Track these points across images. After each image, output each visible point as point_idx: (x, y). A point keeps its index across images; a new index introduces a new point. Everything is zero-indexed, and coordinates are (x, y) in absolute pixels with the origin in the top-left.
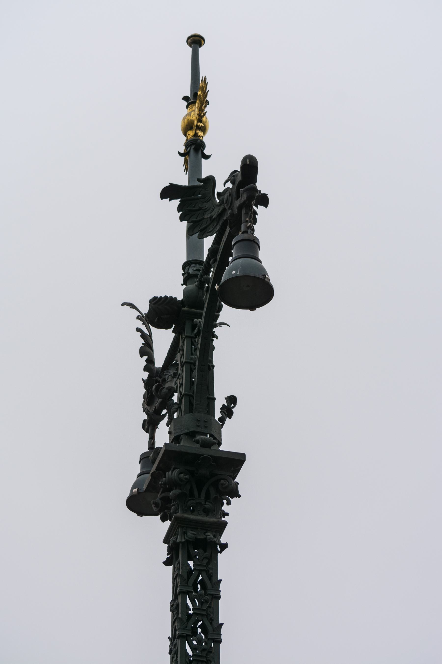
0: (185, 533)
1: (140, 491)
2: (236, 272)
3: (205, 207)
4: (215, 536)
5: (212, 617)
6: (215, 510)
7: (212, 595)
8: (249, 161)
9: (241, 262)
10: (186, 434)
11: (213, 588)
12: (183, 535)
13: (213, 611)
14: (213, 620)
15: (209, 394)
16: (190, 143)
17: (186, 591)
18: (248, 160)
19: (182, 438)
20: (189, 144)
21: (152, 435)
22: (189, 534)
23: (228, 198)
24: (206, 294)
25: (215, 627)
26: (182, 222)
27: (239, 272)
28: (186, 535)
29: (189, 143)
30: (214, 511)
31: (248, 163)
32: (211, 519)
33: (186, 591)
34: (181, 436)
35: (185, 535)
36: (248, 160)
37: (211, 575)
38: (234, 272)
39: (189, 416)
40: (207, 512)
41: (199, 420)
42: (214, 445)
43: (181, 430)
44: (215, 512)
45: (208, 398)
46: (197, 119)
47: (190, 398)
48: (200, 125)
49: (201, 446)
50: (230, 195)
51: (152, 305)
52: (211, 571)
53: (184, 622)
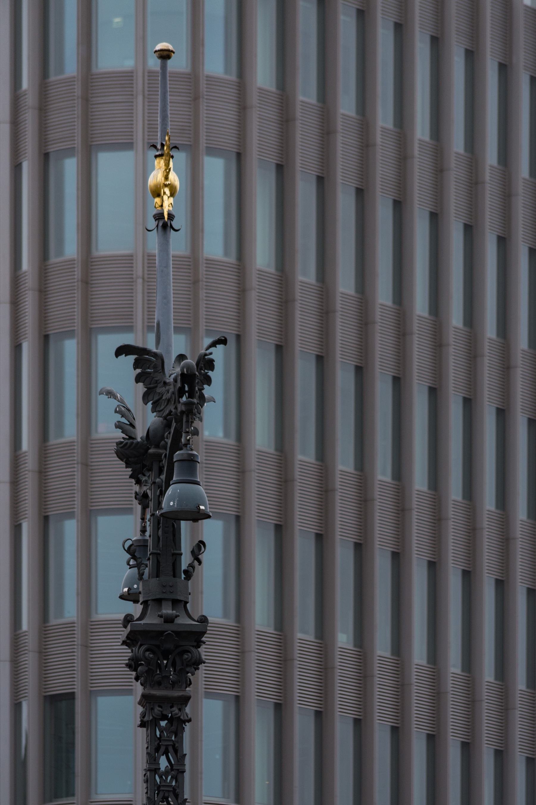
0: (152, 709)
1: (131, 592)
2: (174, 504)
3: (157, 377)
4: (180, 710)
5: (178, 792)
6: (181, 681)
7: (178, 770)
8: (186, 371)
9: (178, 491)
10: (153, 600)
11: (179, 763)
12: (151, 712)
13: (179, 785)
14: (178, 795)
15: (176, 549)
16: (158, 217)
17: (154, 769)
18: (185, 370)
19: (149, 605)
20: (156, 217)
21: (144, 516)
22: (156, 710)
23: (172, 395)
24: (165, 460)
25: (180, 803)
26: (138, 384)
27: (176, 504)
28: (154, 711)
29: (156, 216)
30: (180, 682)
31: (185, 372)
32: (176, 693)
33: (154, 769)
34: (149, 602)
35: (153, 711)
36: (185, 370)
37: (177, 748)
38: (172, 504)
39: (154, 581)
40: (174, 685)
41: (164, 585)
42: (178, 617)
43: (149, 595)
44: (181, 684)
45: (174, 554)
46: (164, 176)
47: (157, 558)
48: (167, 184)
49: (165, 622)
50: (173, 393)
51: (119, 448)
52: (176, 745)
53: (152, 800)
